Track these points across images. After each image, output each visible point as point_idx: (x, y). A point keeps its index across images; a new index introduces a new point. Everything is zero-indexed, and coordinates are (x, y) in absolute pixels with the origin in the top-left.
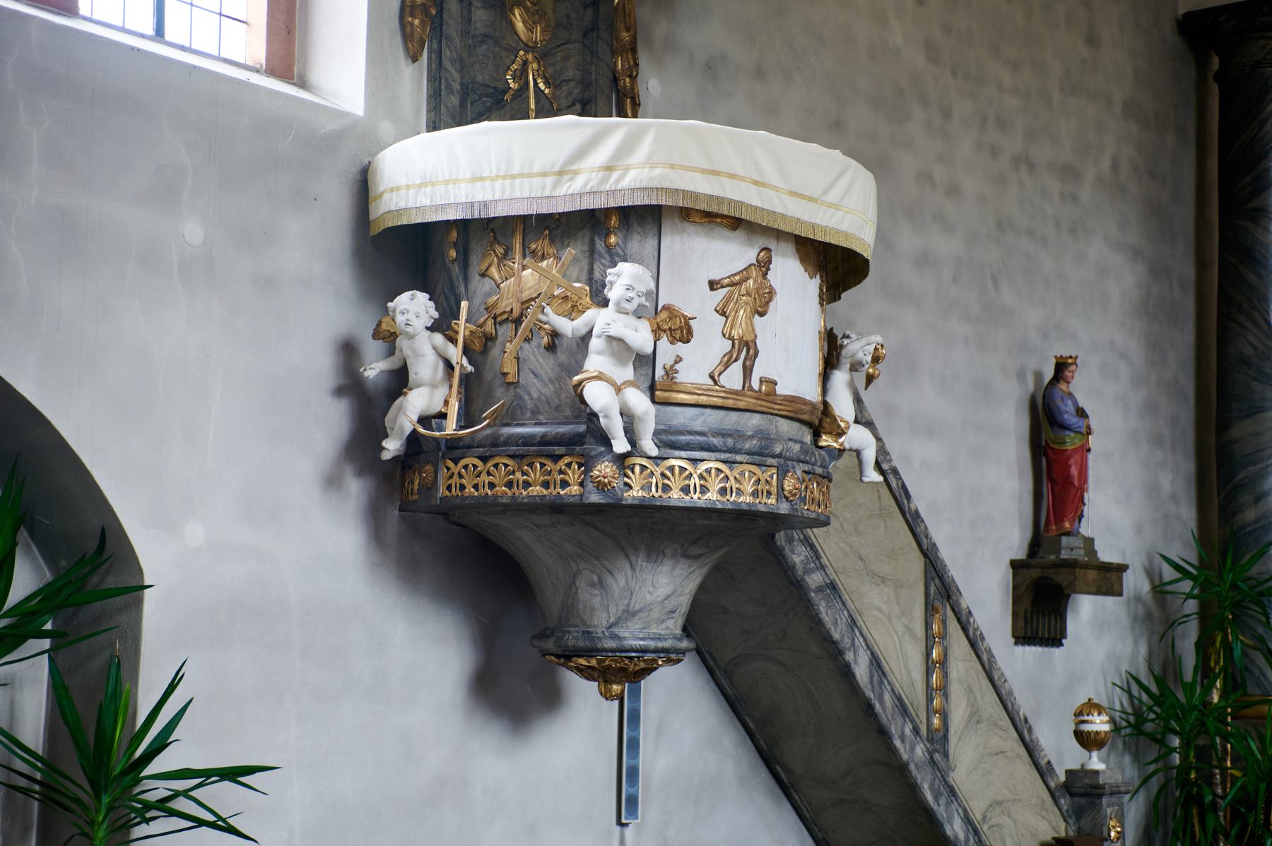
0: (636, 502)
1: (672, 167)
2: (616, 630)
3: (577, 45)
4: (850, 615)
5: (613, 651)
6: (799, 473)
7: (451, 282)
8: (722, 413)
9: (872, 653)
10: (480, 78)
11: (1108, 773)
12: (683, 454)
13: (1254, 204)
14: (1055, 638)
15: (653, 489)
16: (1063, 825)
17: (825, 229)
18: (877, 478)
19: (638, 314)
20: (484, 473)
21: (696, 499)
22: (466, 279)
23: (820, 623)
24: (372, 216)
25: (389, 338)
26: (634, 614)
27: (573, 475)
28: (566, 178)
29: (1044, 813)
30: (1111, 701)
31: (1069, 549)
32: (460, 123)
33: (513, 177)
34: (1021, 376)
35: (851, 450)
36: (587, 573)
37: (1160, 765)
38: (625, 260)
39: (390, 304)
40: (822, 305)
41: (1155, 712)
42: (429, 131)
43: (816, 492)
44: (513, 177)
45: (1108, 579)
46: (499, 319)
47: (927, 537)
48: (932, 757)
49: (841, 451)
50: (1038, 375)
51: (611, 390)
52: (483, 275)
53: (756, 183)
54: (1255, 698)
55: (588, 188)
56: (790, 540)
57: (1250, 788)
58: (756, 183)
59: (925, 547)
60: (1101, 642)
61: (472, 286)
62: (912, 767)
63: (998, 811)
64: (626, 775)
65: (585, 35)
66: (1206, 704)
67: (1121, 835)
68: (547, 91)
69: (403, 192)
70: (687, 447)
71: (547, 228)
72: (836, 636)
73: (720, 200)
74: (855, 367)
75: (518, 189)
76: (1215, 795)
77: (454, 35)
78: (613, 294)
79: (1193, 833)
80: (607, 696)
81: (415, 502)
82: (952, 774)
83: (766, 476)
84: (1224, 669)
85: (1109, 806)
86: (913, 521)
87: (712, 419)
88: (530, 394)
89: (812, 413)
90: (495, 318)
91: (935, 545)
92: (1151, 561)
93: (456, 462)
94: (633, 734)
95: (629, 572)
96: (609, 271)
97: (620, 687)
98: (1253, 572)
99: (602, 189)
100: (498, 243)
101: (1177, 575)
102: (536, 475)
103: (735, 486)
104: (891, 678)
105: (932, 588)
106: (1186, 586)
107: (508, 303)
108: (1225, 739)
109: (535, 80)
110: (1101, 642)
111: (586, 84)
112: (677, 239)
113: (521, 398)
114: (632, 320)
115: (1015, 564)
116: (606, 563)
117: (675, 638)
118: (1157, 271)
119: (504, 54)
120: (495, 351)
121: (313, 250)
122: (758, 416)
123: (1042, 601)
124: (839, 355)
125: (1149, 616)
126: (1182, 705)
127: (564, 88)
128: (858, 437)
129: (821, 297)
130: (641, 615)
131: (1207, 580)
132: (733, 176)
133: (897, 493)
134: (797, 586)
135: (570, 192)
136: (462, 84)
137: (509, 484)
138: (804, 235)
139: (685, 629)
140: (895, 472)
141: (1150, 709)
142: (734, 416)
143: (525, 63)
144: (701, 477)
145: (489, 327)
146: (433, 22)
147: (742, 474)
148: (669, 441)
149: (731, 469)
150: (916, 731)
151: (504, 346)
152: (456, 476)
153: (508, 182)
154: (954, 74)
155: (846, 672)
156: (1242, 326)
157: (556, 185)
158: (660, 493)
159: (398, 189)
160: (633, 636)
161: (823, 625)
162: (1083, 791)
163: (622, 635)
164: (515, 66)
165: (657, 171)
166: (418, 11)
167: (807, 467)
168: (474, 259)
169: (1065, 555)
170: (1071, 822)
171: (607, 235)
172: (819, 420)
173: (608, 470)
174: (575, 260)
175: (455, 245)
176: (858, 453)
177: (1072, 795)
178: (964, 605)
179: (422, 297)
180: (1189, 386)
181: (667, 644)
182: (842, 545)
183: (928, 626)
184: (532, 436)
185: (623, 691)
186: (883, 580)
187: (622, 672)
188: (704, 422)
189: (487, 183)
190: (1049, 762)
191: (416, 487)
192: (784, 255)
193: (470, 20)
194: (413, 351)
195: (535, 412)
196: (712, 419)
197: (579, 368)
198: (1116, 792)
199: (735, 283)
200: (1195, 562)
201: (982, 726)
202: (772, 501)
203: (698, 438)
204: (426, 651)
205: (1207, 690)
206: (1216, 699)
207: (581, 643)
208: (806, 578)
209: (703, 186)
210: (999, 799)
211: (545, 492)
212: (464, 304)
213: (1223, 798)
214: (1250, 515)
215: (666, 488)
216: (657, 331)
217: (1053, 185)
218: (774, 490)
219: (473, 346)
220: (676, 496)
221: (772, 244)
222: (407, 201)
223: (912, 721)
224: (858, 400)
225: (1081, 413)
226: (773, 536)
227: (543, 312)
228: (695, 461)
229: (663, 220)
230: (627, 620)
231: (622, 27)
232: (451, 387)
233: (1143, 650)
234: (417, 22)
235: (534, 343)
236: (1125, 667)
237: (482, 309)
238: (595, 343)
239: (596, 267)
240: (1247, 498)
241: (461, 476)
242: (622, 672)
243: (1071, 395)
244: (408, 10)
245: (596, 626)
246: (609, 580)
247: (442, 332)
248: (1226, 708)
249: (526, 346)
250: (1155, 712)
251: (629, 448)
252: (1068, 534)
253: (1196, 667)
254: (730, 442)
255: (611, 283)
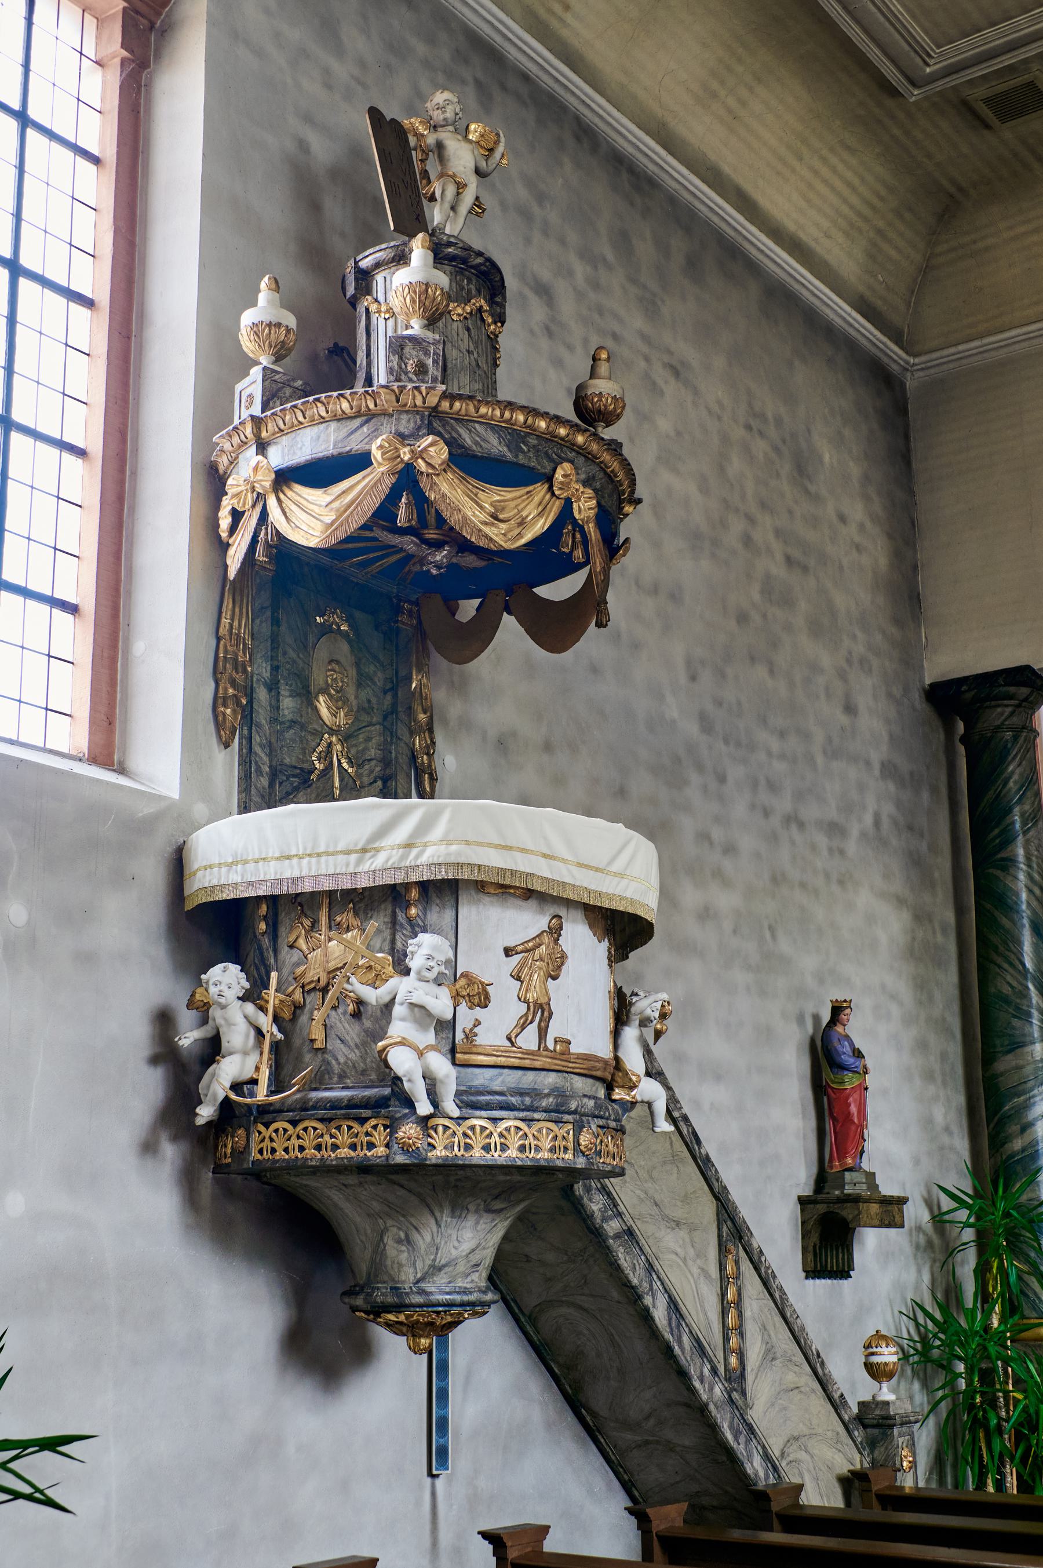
0: (440, 1161)
1: (468, 843)
2: (422, 1285)
3: (378, 727)
4: (648, 1260)
5: (421, 1306)
6: (594, 1127)
7: (262, 953)
8: (520, 1073)
9: (670, 1297)
10: (287, 761)
11: (898, 1403)
12: (484, 1113)
13: (1003, 855)
14: (843, 1272)
15: (456, 1148)
16: (858, 1457)
17: (611, 897)
18: (668, 1127)
19: (438, 982)
20: (294, 1137)
21: (497, 1157)
22: (276, 951)
23: (619, 1268)
24: (186, 893)
25: (203, 1010)
26: (440, 1269)
27: (380, 1137)
28: (368, 855)
29: (839, 1446)
30: (898, 1329)
31: (853, 1185)
32: (270, 806)
33: (319, 855)
34: (800, 1019)
35: (642, 1102)
36: (394, 1230)
37: (947, 1391)
38: (425, 931)
39: (203, 976)
40: (611, 966)
41: (940, 1339)
42: (239, 813)
43: (611, 1146)
44: (319, 855)
45: (890, 1212)
46: (307, 988)
47: (717, 1180)
48: (730, 1396)
49: (634, 1104)
50: (816, 1018)
51: (413, 1055)
52: (291, 947)
53: (545, 856)
54: (1032, 1321)
55: (389, 865)
56: (588, 1189)
57: (1032, 1411)
58: (545, 856)
59: (716, 1190)
60: (887, 1270)
61: (281, 957)
62: (712, 1407)
63: (795, 1446)
64: (437, 1425)
65: (385, 718)
66: (987, 1328)
67: (914, 1464)
68: (350, 770)
69: (216, 870)
70: (487, 1107)
71: (352, 901)
72: (635, 1281)
73: (513, 873)
74: (644, 1023)
75: (323, 866)
76: (1000, 1418)
77: (264, 722)
78: (415, 963)
79: (981, 1456)
80: (416, 1350)
81: (228, 1165)
82: (750, 1412)
83: (563, 1132)
84: (1002, 1295)
85: (900, 1436)
86: (704, 1166)
87: (511, 1079)
88: (337, 1060)
89: (605, 1069)
90: (303, 987)
91: (725, 1188)
92: (929, 1192)
93: (267, 1125)
94: (442, 1384)
95: (435, 1228)
96: (410, 942)
97: (428, 1341)
98: (1024, 1198)
99: (403, 864)
100: (306, 916)
101: (954, 1205)
102: (343, 1138)
103: (534, 1143)
104: (689, 1320)
105: (725, 1229)
106: (963, 1215)
107: (314, 973)
108: (1006, 1363)
109: (339, 761)
110: (887, 1270)
111: (386, 762)
112: (474, 910)
113: (329, 1063)
114: (432, 988)
115: (803, 1201)
116: (413, 1220)
117: (480, 1291)
118: (921, 917)
119: (309, 738)
120: (304, 1019)
121: (129, 923)
122: (553, 1074)
123: (830, 1235)
124: (628, 1012)
125: (930, 1244)
126: (965, 1331)
127: (367, 767)
128: (650, 1089)
129: (609, 959)
130: (447, 1269)
131: (981, 1209)
132: (523, 851)
133: (688, 1140)
134: (596, 1234)
135: (373, 868)
136: (270, 767)
137: (318, 1147)
138: (592, 903)
139: (490, 1278)
140: (686, 1118)
141: (935, 1336)
142: (531, 1075)
143: (330, 745)
144: (501, 1135)
145: (298, 996)
146: (243, 711)
147: (540, 1131)
148: (470, 1101)
149: (529, 1127)
150: (714, 1371)
151: (312, 1014)
152: (267, 1140)
153: (314, 860)
154: (726, 742)
155: (646, 1316)
156: (1000, 967)
157: (359, 862)
158: (462, 1152)
159: (211, 867)
160: (439, 1289)
161: (622, 1271)
162: (875, 1422)
163: (429, 1290)
164: (320, 749)
165: (454, 848)
166: (230, 702)
167: (601, 1122)
168: (283, 931)
169: (848, 1190)
170: (865, 1453)
171: (408, 906)
172: (611, 1075)
173: (412, 1131)
174: (379, 931)
175: (265, 918)
176: (650, 1105)
177: (865, 1427)
178: (755, 1246)
179: (234, 969)
180: (955, 1023)
181: (472, 1298)
182: (638, 1192)
183: (722, 1267)
184: (339, 1100)
185: (431, 1344)
186: (678, 1224)
187: (431, 1327)
188: (503, 1082)
189: (295, 861)
190: (842, 1395)
191: (229, 1150)
192: (574, 921)
193: (278, 708)
194: (226, 1020)
195: (342, 1077)
196: (511, 1079)
197: (382, 1034)
198: (906, 1422)
199: (529, 949)
200: (970, 1192)
201: (777, 1362)
202: (569, 1156)
203: (497, 1097)
204: (240, 1309)
205: (987, 1315)
206: (995, 1323)
207: (390, 1300)
208: (605, 1225)
209: (496, 859)
210: (796, 1434)
211: (353, 1154)
212: (274, 975)
213: (1007, 1421)
214: (1017, 1144)
215: (468, 1147)
216: (456, 997)
217: (822, 840)
218: (571, 1145)
219: (283, 1015)
220: (477, 1155)
221: (562, 912)
222: (219, 879)
223: (710, 1361)
224: (648, 1053)
225: (858, 1054)
226: (572, 1186)
227: (348, 982)
228: (494, 1120)
229: (460, 892)
230: (433, 1274)
231: (420, 708)
232: (261, 1053)
233: (926, 1278)
234: (228, 711)
235: (340, 1010)
236: (910, 1295)
237: (290, 979)
238: (398, 1010)
239: (397, 937)
240: (1015, 1128)
241: (272, 1140)
242: (431, 1327)
243: (847, 1037)
244: (220, 701)
245: (404, 1282)
246: (415, 1236)
247: (253, 1002)
248: (1004, 1332)
249: (333, 1013)
250: (940, 1339)
251: (432, 1110)
252: (850, 1170)
253: (976, 1295)
254: (528, 1100)
255: (412, 953)
